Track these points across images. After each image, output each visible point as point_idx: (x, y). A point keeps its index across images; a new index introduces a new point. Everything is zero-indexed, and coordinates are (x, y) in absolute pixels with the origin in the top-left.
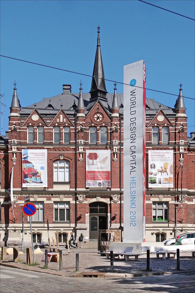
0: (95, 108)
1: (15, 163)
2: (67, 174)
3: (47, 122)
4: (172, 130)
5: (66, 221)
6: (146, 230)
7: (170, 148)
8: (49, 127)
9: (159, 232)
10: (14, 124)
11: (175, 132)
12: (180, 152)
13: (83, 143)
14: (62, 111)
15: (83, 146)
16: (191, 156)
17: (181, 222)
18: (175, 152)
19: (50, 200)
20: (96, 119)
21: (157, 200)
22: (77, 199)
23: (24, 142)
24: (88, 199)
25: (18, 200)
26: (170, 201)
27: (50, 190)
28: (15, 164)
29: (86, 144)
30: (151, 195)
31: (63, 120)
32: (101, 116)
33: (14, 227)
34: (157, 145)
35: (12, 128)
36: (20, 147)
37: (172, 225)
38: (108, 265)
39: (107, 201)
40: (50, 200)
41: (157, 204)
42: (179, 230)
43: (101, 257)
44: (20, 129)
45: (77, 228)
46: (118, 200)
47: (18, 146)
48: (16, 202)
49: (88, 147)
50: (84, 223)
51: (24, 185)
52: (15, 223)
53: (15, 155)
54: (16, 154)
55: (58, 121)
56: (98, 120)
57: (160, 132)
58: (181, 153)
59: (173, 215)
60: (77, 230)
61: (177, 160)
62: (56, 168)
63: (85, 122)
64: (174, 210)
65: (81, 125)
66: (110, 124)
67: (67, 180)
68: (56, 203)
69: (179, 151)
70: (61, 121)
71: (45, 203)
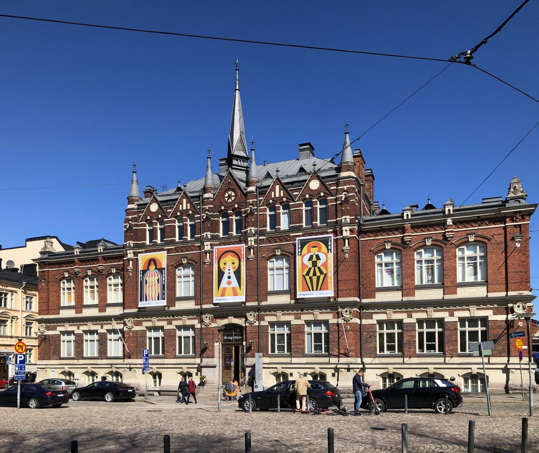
0: (225, 183)
1: (131, 274)
2: (192, 285)
3: (332, 190)
4: (332, 201)
5: (397, 352)
6: (264, 368)
7: (291, 235)
8: (170, 219)
9: (387, 371)
10: (207, 210)
11: (335, 203)
12: (343, 237)
13: (209, 237)
14: (278, 179)
15: (210, 241)
16: (495, 229)
17: (346, 355)
18: (336, 238)
19: (300, 318)
20: (226, 199)
21: (310, 317)
22: (203, 322)
23: (141, 244)
24: (217, 320)
25: (135, 325)
26: (166, 326)
27: (172, 309)
28: (131, 275)
29: (214, 238)
30: (302, 310)
32: (233, 194)
33: (346, 364)
34: (311, 229)
35: (342, 197)
36: (137, 251)
37: (334, 360)
38: (5, 411)
39: (240, 321)
40: (300, 318)
41: (312, 325)
42: (344, 368)
43: (375, 416)
44: (136, 225)
45: (201, 365)
46: (255, 321)
47: (212, 241)
48: (131, 329)
49: (218, 242)
50: (212, 358)
51: (141, 304)
52: (131, 358)
53: (347, 241)
54: (348, 239)
55: (273, 196)
56: (230, 200)
57: (314, 206)
58: (345, 238)
59: (335, 342)
60: (203, 368)
61: (339, 251)
62: (272, 269)
63: (212, 206)
64: (336, 335)
65: (347, 191)
66: (244, 204)
67: (192, 294)
68: (179, 328)
69: (342, 235)
70: (277, 195)
71: (165, 328)
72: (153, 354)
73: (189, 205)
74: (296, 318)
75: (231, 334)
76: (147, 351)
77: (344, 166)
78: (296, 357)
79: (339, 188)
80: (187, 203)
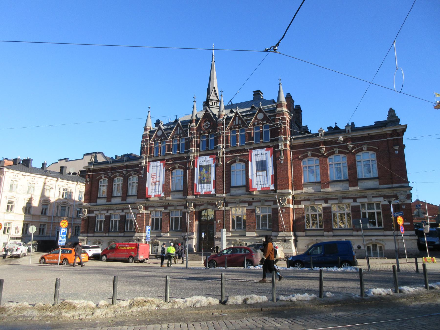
19: (252, 205)
31: (180, 132)
40: (252, 205)
72: (98, 231)
73: (181, 130)
74: (165, 209)
75: (377, 253)
76: (149, 227)
77: (226, 314)
78: (249, 232)
79: (276, 118)
80: (180, 130)
